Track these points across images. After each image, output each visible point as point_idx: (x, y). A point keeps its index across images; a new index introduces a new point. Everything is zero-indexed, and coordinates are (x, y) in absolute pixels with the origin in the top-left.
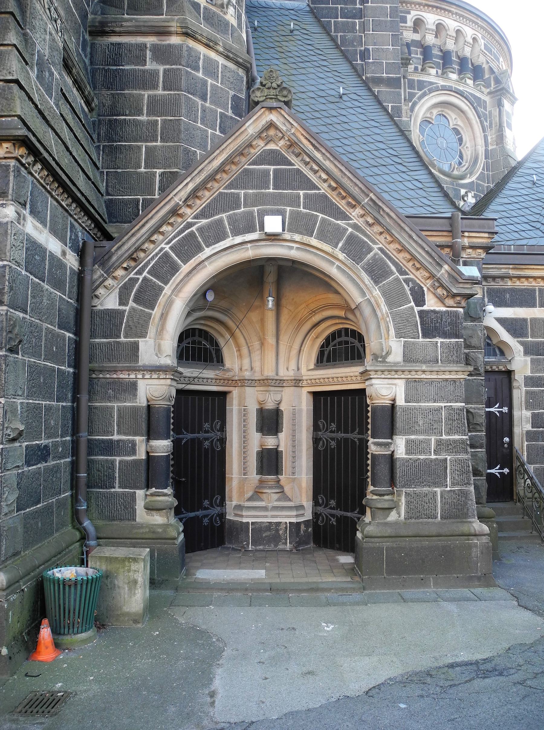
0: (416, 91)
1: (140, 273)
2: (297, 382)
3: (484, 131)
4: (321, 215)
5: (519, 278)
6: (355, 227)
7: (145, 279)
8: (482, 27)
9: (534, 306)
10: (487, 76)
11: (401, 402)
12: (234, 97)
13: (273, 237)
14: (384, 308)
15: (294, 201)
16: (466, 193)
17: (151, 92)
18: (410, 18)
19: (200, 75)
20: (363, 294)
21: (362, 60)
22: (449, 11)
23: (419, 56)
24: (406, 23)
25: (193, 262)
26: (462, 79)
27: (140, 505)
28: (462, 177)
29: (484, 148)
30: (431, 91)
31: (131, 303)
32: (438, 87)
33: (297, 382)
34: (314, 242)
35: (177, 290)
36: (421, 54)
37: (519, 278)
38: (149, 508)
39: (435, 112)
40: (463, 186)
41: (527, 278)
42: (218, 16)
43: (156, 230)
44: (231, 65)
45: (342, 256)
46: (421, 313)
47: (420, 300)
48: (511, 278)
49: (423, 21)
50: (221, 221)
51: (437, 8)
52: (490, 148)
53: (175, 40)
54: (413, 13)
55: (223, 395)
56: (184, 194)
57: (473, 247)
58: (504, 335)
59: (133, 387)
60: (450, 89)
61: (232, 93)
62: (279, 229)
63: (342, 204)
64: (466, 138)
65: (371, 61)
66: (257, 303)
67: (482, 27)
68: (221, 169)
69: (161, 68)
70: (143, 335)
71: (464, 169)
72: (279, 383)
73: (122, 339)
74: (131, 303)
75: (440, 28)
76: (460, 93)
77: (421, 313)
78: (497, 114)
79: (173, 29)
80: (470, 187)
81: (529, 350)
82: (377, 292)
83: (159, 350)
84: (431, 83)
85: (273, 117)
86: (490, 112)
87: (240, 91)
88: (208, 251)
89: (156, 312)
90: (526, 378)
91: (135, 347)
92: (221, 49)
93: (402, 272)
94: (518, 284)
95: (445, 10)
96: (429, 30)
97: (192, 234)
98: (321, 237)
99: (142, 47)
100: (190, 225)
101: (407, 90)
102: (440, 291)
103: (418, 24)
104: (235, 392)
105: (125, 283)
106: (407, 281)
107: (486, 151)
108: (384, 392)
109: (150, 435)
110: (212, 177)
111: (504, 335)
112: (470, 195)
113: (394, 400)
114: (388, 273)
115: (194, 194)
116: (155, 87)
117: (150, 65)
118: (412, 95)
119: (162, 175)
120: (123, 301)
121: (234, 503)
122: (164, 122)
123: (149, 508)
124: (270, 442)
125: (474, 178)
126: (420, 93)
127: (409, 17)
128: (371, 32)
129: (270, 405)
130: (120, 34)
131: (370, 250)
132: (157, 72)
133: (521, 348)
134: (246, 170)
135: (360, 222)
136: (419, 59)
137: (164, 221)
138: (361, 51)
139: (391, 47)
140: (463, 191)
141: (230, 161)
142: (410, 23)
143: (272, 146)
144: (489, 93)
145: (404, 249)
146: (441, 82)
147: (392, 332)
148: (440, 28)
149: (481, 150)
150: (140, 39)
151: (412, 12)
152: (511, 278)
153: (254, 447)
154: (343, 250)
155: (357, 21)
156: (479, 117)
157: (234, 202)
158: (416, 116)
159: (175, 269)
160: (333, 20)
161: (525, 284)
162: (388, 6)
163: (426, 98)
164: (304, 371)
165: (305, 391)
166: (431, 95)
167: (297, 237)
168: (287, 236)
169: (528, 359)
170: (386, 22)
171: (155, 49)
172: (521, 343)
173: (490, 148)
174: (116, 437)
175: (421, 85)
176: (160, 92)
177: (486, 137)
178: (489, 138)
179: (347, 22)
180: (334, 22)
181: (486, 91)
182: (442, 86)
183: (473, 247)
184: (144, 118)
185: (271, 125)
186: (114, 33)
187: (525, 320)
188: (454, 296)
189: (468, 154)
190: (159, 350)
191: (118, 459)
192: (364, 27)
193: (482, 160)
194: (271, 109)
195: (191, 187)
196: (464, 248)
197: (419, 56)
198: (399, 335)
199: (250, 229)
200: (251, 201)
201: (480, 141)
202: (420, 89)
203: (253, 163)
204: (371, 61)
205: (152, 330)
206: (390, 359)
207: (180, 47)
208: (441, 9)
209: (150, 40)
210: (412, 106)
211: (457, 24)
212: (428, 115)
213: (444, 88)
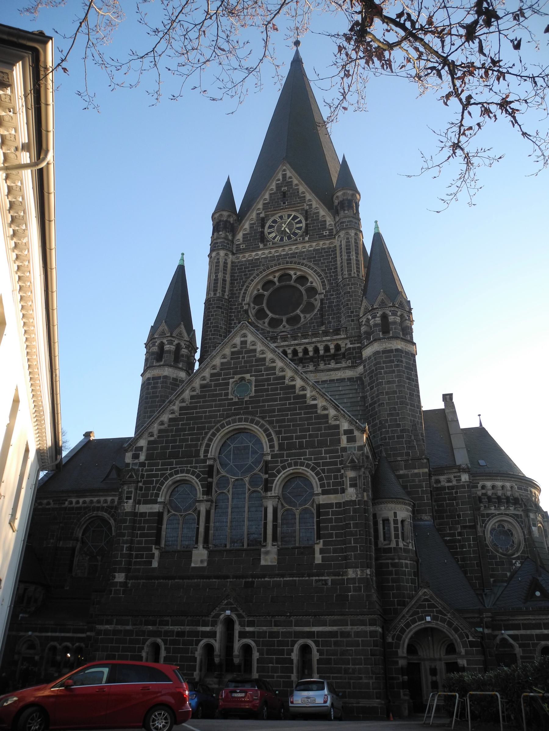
1: (397, 632)
2: (440, 660)
3: (522, 529)
4: (440, 615)
5: (513, 620)
6: (449, 618)
7: (398, 634)
8: (514, 481)
9: (520, 629)
10: (520, 502)
11: (466, 665)
13: (429, 622)
14: (459, 640)
15: (433, 612)
16: (516, 562)
17: (392, 577)
18: (480, 485)
20: (453, 636)
21: (458, 518)
24: (478, 488)
25: (409, 629)
26: (507, 507)
27: (402, 694)
28: (513, 554)
29: (523, 537)
30: (493, 517)
31: (395, 640)
33: (440, 660)
34: (439, 623)
35: (406, 637)
37: (513, 620)
38: (404, 695)
39: (497, 525)
40: (514, 559)
41: (516, 620)
43: (400, 621)
44: (412, 562)
45: (446, 626)
46: (468, 641)
47: (468, 638)
48: (511, 620)
50: (415, 618)
51: (491, 479)
52: (527, 537)
53: (397, 561)
54: (481, 483)
55: (418, 665)
56: (406, 612)
57: (487, 617)
58: (511, 641)
59: (397, 662)
60: (502, 514)
62: (430, 620)
63: (445, 612)
64: (514, 532)
67: (514, 481)
68: (414, 604)
70: (399, 648)
71: (515, 548)
72: (435, 660)
73: (394, 650)
74: (395, 640)
76: (507, 515)
77: (468, 641)
78: (527, 520)
80: (517, 558)
81: (521, 646)
82: (456, 636)
83: (403, 652)
85: (425, 590)
86: (524, 519)
88: (413, 626)
89: (401, 642)
90: (521, 656)
91: (397, 652)
93: (463, 630)
94: (514, 622)
97: (408, 622)
98: (441, 621)
99: (388, 563)
100: (408, 619)
101: (481, 519)
102: (473, 635)
103: (483, 487)
104: (422, 663)
106: (464, 632)
107: (525, 539)
108: (461, 663)
109: (403, 675)
110: (412, 607)
111: (511, 641)
112: (517, 563)
113: (436, 666)
114: (459, 630)
115: (408, 611)
116: (393, 575)
117: (390, 569)
119: (397, 600)
120: (393, 640)
121: (425, 698)
122: (396, 585)
123: (404, 695)
124: (434, 678)
125: (519, 554)
126: (488, 519)
127: (479, 485)
129: (433, 667)
131: (453, 624)
132: (392, 571)
133: (518, 645)
134: (420, 604)
135: (450, 617)
137: (401, 619)
140: (514, 561)
141: (416, 602)
143: (426, 597)
144: (522, 511)
145: (462, 624)
146: (497, 512)
147: (461, 646)
149: (522, 538)
150: (387, 561)
152: (511, 620)
153: (430, 681)
154: (447, 625)
156: (519, 523)
157: (417, 613)
158: (487, 530)
159: (405, 631)
161: (516, 622)
163: (491, 520)
164: (442, 656)
165: (443, 662)
167: (435, 622)
168: (432, 621)
169: (521, 649)
171: (392, 564)
172: (518, 644)
173: (527, 537)
174: (394, 676)
175: (488, 515)
176: (394, 576)
177: (524, 532)
178: (525, 532)
181: (521, 509)
183: (487, 617)
184: (390, 584)
185: (425, 592)
187: (518, 635)
188: (476, 636)
189: (516, 541)
190: (403, 652)
191: (395, 682)
192: (457, 504)
193: (523, 543)
194: (425, 588)
195: (407, 610)
196: (484, 618)
198: (463, 647)
199: (423, 620)
200: (422, 612)
201: (521, 534)
203: (422, 602)
205: (401, 647)
206: (462, 654)
208: (493, 479)
209: (390, 561)
212: (494, 526)
213: (499, 514)
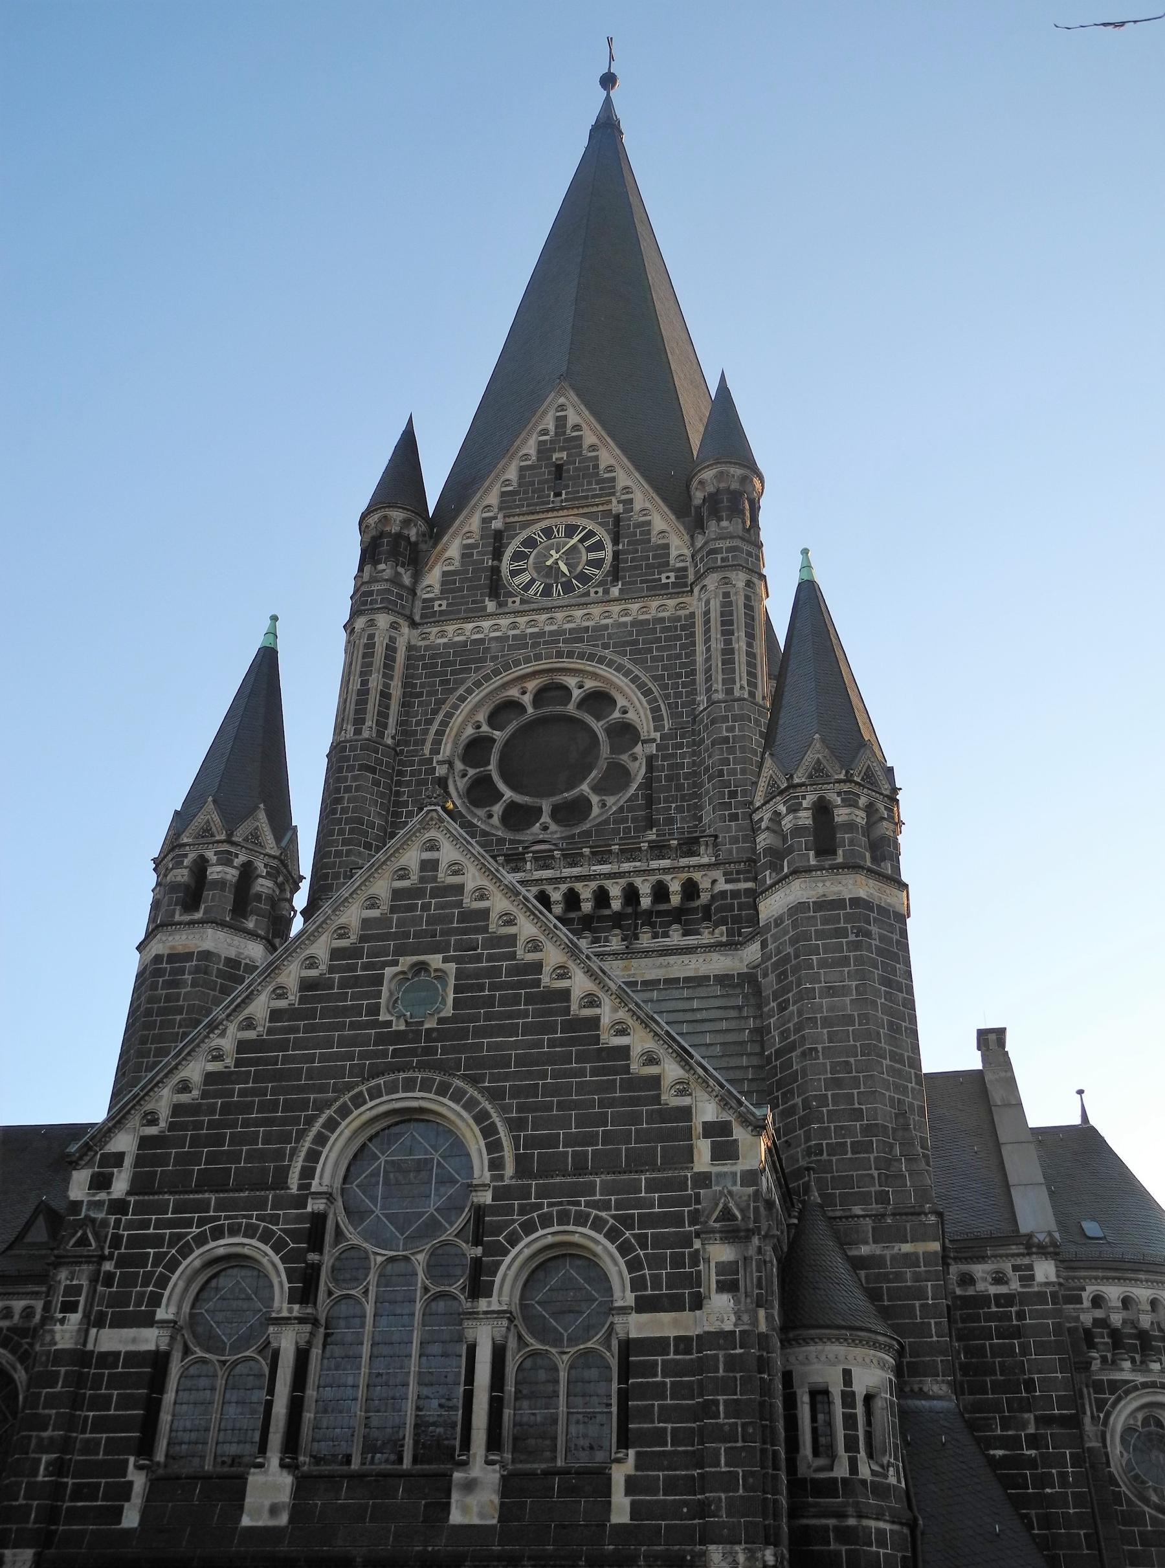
0: (1107, 1396)
12: (904, 1558)
19: (874, 1549)
21: (1027, 1391)
22: (1136, 1280)
23: (1106, 1340)
30: (1127, 1393)
32: (1136, 1385)
36: (1108, 1337)
39: (1140, 1416)
42: (882, 1484)
49: (1103, 1297)
53: (852, 1522)
54: (1089, 1289)
60: (1153, 1385)
61: (900, 1554)
65: (1038, 1394)
66: (870, 1390)
69: (844, 1548)
75: (1126, 1302)
79: (850, 1513)
84: (1127, 1382)
87: (906, 1551)
92: (888, 1518)
95: (1130, 1280)
96: (1113, 1308)
99: (826, 1528)
105: (361, 1225)
118: (1101, 1404)
127: (1085, 1295)
128: (1034, 1357)
130: (807, 1517)
136: (1107, 1343)
138: (1024, 1380)
139: (1059, 1375)
142: (1087, 1303)
146: (1140, 1379)
148: (1126, 1302)
150: (824, 1521)
151: (1087, 1287)
155: (1016, 1341)
160: (987, 1343)
162: (1050, 1321)
163: (1123, 1403)
166: (1129, 1398)
170: (1050, 1342)
175: (1114, 1386)
179: (1004, 1343)
180: (990, 1344)
182: (1141, 1383)
186: (803, 1517)
197: (1106, 1340)
202: (1112, 1393)
204: (1038, 1394)
207: (855, 1528)
208: (1125, 1279)
210: (1104, 1417)
211: (1150, 1292)
212: (1132, 1422)
213: (1145, 1385)
